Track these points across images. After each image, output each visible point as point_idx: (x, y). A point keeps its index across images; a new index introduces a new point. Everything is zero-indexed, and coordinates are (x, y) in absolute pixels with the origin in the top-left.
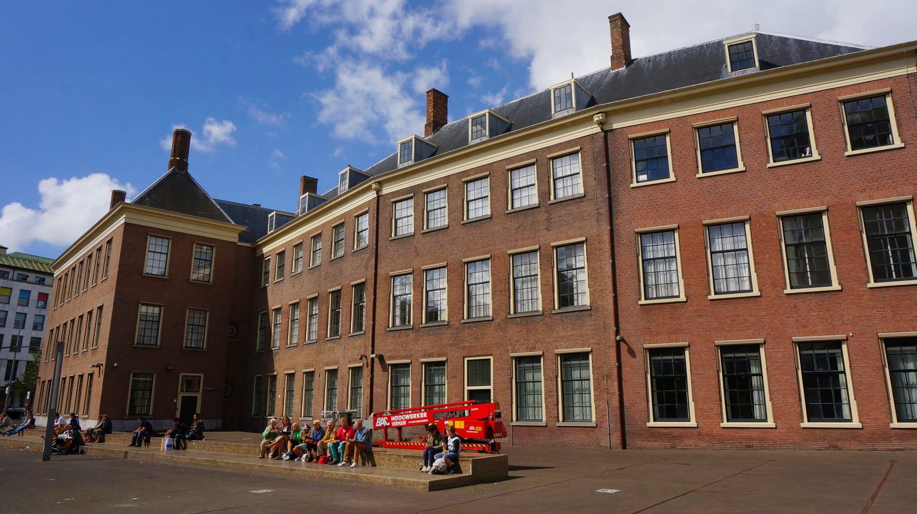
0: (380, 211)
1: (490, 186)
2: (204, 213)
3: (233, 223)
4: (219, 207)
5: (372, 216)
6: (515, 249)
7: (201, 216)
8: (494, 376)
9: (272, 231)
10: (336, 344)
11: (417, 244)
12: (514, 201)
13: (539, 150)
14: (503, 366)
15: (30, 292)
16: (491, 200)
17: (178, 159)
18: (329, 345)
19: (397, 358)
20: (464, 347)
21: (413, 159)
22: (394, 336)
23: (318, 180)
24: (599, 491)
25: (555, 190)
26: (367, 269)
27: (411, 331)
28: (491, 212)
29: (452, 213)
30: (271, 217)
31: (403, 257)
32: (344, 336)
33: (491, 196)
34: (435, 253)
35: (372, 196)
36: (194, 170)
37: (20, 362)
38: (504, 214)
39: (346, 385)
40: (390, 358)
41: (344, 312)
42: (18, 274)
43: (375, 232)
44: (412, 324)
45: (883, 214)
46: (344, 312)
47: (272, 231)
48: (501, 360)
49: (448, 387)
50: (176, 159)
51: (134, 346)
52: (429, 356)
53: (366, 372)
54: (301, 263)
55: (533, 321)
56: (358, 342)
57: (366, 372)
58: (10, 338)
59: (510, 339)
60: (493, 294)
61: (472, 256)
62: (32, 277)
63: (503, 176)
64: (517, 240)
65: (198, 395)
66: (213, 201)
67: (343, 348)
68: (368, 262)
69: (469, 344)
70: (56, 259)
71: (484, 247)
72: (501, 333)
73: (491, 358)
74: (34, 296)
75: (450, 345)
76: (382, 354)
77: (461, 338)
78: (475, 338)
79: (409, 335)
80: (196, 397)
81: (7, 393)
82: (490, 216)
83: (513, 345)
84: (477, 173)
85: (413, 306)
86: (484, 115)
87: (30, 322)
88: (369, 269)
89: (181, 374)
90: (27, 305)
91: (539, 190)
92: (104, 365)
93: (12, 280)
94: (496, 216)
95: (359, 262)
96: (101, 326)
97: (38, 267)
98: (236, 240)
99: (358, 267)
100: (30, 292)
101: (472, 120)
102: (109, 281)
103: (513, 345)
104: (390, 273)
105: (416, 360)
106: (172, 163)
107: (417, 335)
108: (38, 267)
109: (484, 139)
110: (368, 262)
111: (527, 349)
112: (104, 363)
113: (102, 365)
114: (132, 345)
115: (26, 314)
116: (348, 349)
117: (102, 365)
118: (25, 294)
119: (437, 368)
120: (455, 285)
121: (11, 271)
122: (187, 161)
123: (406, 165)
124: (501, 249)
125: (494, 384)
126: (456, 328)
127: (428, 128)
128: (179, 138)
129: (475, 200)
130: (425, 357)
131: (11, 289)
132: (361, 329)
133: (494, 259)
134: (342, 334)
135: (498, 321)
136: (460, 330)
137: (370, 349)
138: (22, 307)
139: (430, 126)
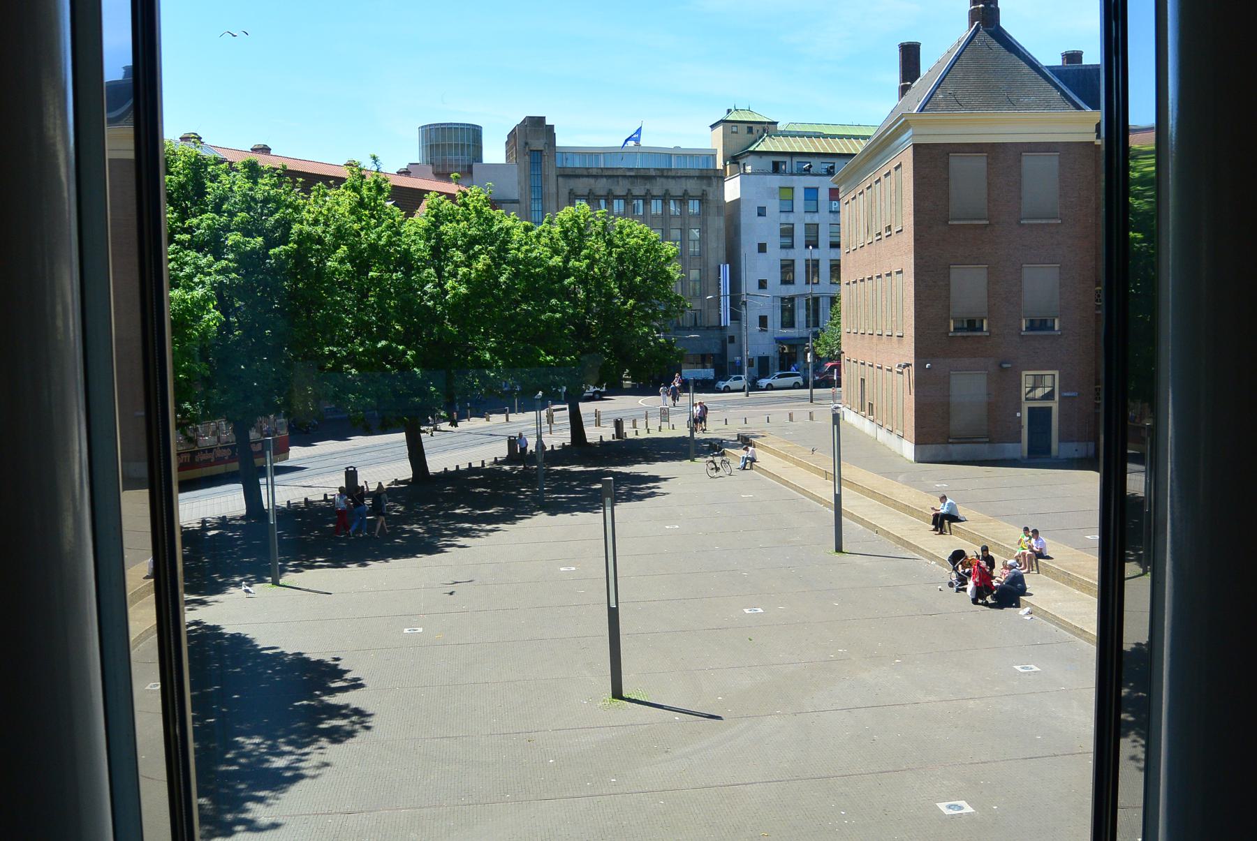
15: (817, 189)
24: (1088, 537)
37: (821, 299)
42: (798, 162)
45: (1170, 390)
51: (950, 335)
58: (804, 263)
65: (1055, 404)
80: (1050, 409)
81: (809, 361)
90: (817, 211)
93: (792, 174)
100: (817, 189)
112: (912, 361)
113: (911, 365)
114: (947, 334)
115: (818, 225)
117: (911, 365)
118: (811, 193)
121: (787, 159)
131: (793, 188)
138: (812, 214)
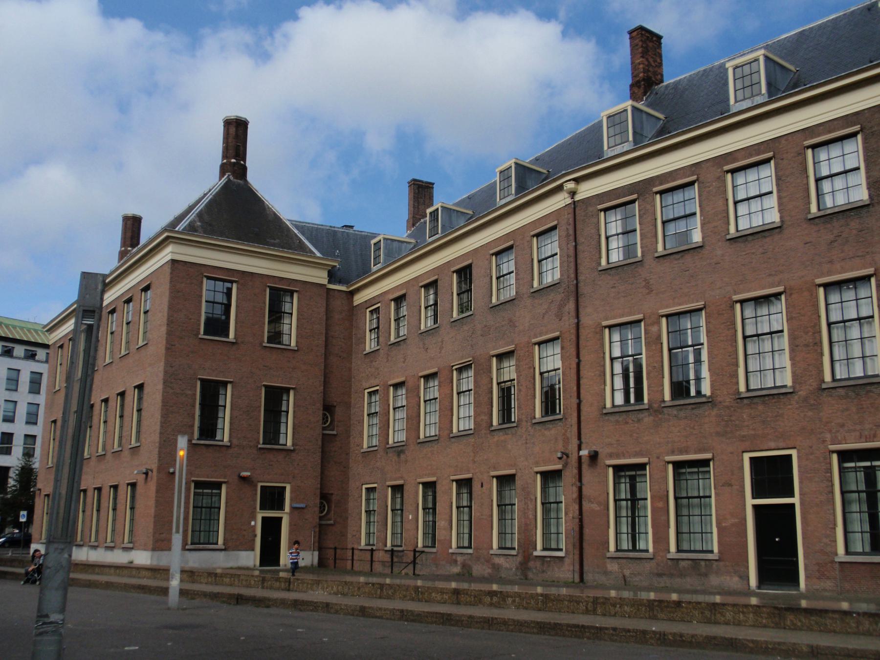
0: (578, 226)
1: (776, 176)
2: (277, 241)
3: (318, 254)
4: (296, 231)
5: (564, 234)
6: (828, 276)
7: (274, 245)
8: (801, 482)
9: (379, 266)
10: (510, 436)
11: (649, 275)
12: (610, 252)
13: (866, 111)
14: (816, 466)
16: (780, 198)
17: (234, 162)
18: (499, 437)
19: (624, 456)
20: (744, 436)
21: (631, 138)
22: (617, 421)
23: (433, 184)
25: (608, 250)
26: (559, 316)
27: (646, 413)
28: (781, 217)
29: (709, 222)
30: (375, 244)
31: (624, 297)
32: (524, 423)
33: (779, 191)
34: (681, 289)
35: (563, 202)
36: (255, 178)
38: (386, 344)
39: (531, 500)
40: (611, 456)
41: (522, 385)
43: (572, 259)
44: (646, 401)
46: (522, 385)
47: (379, 266)
48: (811, 457)
49: (716, 500)
50: (231, 162)
52: (681, 452)
53: (570, 475)
54: (404, 323)
55: (870, 391)
56: (552, 432)
57: (570, 475)
59: (827, 423)
60: (792, 351)
61: (749, 291)
62: (19, 350)
63: (800, 157)
64: (831, 262)
66: (288, 223)
67: (524, 442)
68: (561, 306)
69: (753, 432)
70: (45, 323)
71: (770, 275)
72: (810, 414)
73: (794, 453)
74: (25, 379)
75: (718, 434)
76: (598, 450)
77: (737, 422)
78: (763, 422)
79: (642, 419)
82: (779, 225)
83: (834, 431)
84: (751, 156)
85: (648, 374)
86: (756, 60)
87: (22, 412)
88: (565, 318)
89: (260, 484)
91: (868, 178)
92: (155, 471)
94: (790, 223)
95: (546, 307)
96: (143, 413)
97: (33, 336)
98: (325, 281)
99: (544, 315)
101: (734, 69)
102: (151, 349)
103: (834, 431)
104: (603, 323)
105: (658, 458)
106: (223, 169)
107: (657, 419)
108: (33, 336)
109: (759, 100)
110: (561, 306)
111: (861, 438)
112: (154, 467)
116: (534, 443)
117: (152, 471)
119: (696, 470)
120: (722, 338)
122: (245, 162)
123: (619, 150)
124: (803, 277)
125: (801, 494)
126: (728, 407)
127: (636, 90)
128: (232, 130)
129: (748, 199)
130: (673, 453)
132: (554, 412)
133: (791, 294)
134: (520, 420)
135: (802, 393)
136: (735, 410)
137: (575, 442)
139: (639, 87)
